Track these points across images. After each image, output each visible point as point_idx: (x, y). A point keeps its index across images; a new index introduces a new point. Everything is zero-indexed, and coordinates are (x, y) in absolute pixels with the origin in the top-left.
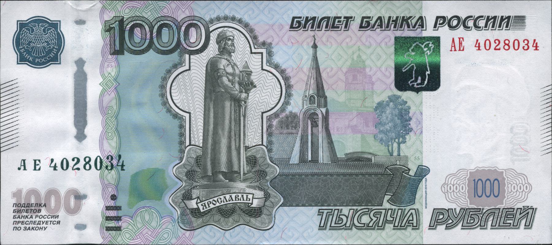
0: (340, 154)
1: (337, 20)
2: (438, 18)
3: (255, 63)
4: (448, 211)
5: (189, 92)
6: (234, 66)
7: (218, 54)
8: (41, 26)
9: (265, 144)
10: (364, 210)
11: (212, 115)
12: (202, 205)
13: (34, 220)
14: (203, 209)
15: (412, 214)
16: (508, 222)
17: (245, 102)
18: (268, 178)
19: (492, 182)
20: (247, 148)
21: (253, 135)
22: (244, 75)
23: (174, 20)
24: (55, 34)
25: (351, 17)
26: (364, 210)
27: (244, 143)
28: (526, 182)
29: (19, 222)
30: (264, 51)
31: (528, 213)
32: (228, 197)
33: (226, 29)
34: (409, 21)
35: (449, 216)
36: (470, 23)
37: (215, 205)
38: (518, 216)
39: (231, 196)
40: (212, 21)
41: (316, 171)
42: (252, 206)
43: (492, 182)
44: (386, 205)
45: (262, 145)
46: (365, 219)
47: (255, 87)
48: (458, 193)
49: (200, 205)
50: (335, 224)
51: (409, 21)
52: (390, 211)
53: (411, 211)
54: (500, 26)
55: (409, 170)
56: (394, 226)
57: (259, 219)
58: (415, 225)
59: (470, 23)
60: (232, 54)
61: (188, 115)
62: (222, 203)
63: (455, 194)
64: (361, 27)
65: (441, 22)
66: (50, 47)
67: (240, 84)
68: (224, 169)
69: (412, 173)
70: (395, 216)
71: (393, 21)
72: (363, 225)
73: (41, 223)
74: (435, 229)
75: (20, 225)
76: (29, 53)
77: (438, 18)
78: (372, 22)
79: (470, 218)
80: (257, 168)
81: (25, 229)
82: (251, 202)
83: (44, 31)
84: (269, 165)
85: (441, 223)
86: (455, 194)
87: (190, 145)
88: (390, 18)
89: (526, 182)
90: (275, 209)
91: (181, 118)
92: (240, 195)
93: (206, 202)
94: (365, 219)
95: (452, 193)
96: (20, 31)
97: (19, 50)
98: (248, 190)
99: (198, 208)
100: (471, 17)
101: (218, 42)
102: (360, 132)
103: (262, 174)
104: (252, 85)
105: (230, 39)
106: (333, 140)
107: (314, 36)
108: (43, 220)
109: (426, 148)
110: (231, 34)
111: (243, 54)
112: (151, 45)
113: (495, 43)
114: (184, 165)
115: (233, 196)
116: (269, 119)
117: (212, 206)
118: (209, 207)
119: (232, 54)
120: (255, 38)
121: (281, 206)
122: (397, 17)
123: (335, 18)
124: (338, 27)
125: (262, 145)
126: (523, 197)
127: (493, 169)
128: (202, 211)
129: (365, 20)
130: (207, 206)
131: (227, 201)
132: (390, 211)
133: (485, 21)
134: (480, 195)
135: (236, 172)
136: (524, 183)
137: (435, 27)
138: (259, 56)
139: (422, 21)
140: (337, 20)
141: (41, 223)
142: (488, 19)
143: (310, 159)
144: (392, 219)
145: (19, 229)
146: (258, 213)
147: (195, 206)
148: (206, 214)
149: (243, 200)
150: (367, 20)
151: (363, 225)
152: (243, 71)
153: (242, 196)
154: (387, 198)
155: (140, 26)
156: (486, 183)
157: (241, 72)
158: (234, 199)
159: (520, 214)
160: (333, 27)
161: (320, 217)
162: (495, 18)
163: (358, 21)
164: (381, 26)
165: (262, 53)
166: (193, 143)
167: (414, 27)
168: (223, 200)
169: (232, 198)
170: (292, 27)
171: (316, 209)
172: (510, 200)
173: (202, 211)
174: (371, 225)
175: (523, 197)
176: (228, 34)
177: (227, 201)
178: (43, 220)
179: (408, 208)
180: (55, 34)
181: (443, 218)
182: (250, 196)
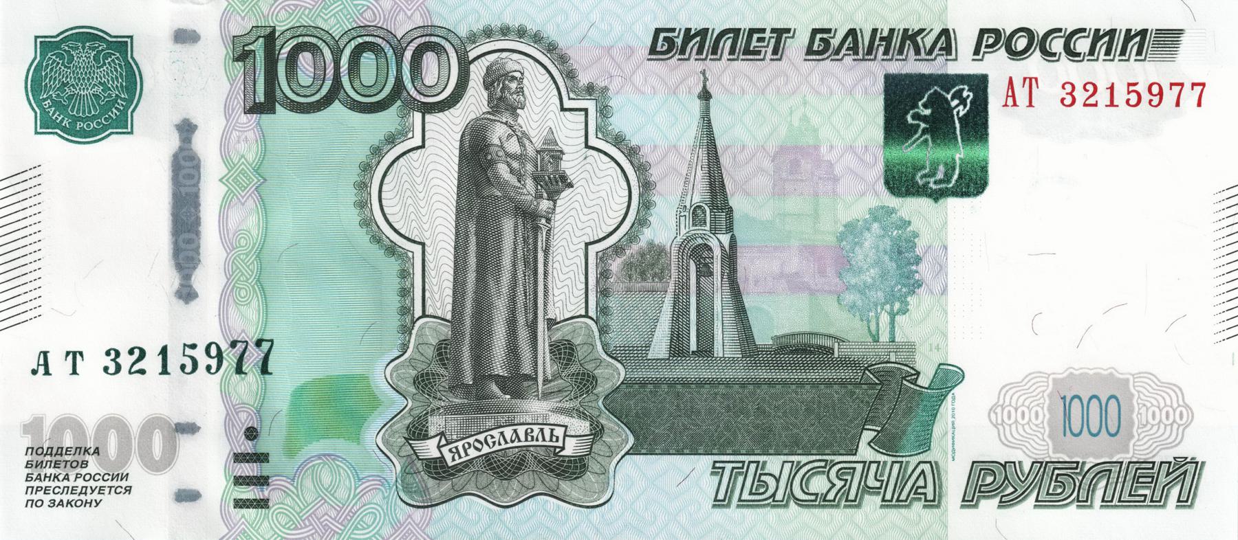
2: (983, 32)
3: (569, 132)
4: (1004, 467)
6: (522, 138)
7: (488, 113)
9: (592, 313)
10: (816, 464)
12: (450, 450)
13: (71, 484)
14: (454, 459)
15: (923, 472)
16: (1141, 492)
17: (548, 220)
18: (599, 389)
20: (551, 323)
22: (547, 158)
24: (120, 66)
25: (788, 31)
26: (816, 464)
27: (545, 313)
29: (38, 489)
30: (590, 105)
31: (1185, 473)
32: (508, 432)
33: (504, 55)
35: (1006, 477)
38: (1163, 480)
39: (515, 431)
40: (473, 38)
44: (865, 452)
46: (819, 484)
47: (570, 185)
49: (445, 450)
51: (919, 39)
52: (874, 466)
54: (1123, 53)
55: (918, 373)
56: (883, 500)
57: (579, 482)
58: (930, 497)
59: (1057, 45)
60: (519, 111)
62: (497, 447)
63: (1020, 427)
64: (810, 51)
65: (991, 41)
67: (536, 179)
68: (499, 369)
69: (924, 381)
70: (885, 478)
71: (882, 39)
72: (813, 498)
73: (89, 491)
74: (976, 506)
75: (40, 495)
77: (983, 32)
78: (835, 42)
79: (1061, 483)
82: (560, 444)
83: (96, 58)
86: (1020, 427)
87: (424, 315)
88: (875, 31)
90: (615, 461)
92: (536, 428)
93: (460, 444)
94: (819, 484)
99: (443, 457)
100: (1060, 30)
101: (488, 85)
104: (564, 182)
105: (514, 78)
106: (747, 305)
107: (704, 73)
110: (517, 67)
111: (542, 114)
113: (1087, 91)
114: (410, 359)
115: (521, 430)
116: (603, 258)
117: (473, 453)
118: (467, 455)
119: (519, 111)
120: (570, 75)
121: (627, 453)
122: (892, 31)
123: (752, 31)
124: (759, 53)
125: (586, 316)
128: (450, 464)
129: (819, 36)
130: (463, 454)
132: (874, 466)
135: (527, 377)
137: (977, 52)
138: (580, 117)
140: (756, 36)
141: (89, 491)
142: (1097, 36)
143: (693, 347)
145: (39, 503)
147: (436, 454)
148: (461, 470)
149: (544, 440)
150: (825, 36)
151: (813, 498)
152: (543, 151)
153: (542, 430)
154: (867, 436)
158: (522, 437)
159: (1168, 474)
160: (747, 51)
161: (717, 479)
162: (1112, 32)
163: (803, 38)
164: (854, 49)
165: (586, 110)
166: (429, 311)
167: (930, 52)
168: (500, 438)
169: (517, 436)
171: (709, 460)
172: (1143, 445)
173: (450, 464)
174: (830, 496)
176: (510, 66)
178: (92, 483)
179: (914, 461)
181: (993, 482)
182: (559, 432)
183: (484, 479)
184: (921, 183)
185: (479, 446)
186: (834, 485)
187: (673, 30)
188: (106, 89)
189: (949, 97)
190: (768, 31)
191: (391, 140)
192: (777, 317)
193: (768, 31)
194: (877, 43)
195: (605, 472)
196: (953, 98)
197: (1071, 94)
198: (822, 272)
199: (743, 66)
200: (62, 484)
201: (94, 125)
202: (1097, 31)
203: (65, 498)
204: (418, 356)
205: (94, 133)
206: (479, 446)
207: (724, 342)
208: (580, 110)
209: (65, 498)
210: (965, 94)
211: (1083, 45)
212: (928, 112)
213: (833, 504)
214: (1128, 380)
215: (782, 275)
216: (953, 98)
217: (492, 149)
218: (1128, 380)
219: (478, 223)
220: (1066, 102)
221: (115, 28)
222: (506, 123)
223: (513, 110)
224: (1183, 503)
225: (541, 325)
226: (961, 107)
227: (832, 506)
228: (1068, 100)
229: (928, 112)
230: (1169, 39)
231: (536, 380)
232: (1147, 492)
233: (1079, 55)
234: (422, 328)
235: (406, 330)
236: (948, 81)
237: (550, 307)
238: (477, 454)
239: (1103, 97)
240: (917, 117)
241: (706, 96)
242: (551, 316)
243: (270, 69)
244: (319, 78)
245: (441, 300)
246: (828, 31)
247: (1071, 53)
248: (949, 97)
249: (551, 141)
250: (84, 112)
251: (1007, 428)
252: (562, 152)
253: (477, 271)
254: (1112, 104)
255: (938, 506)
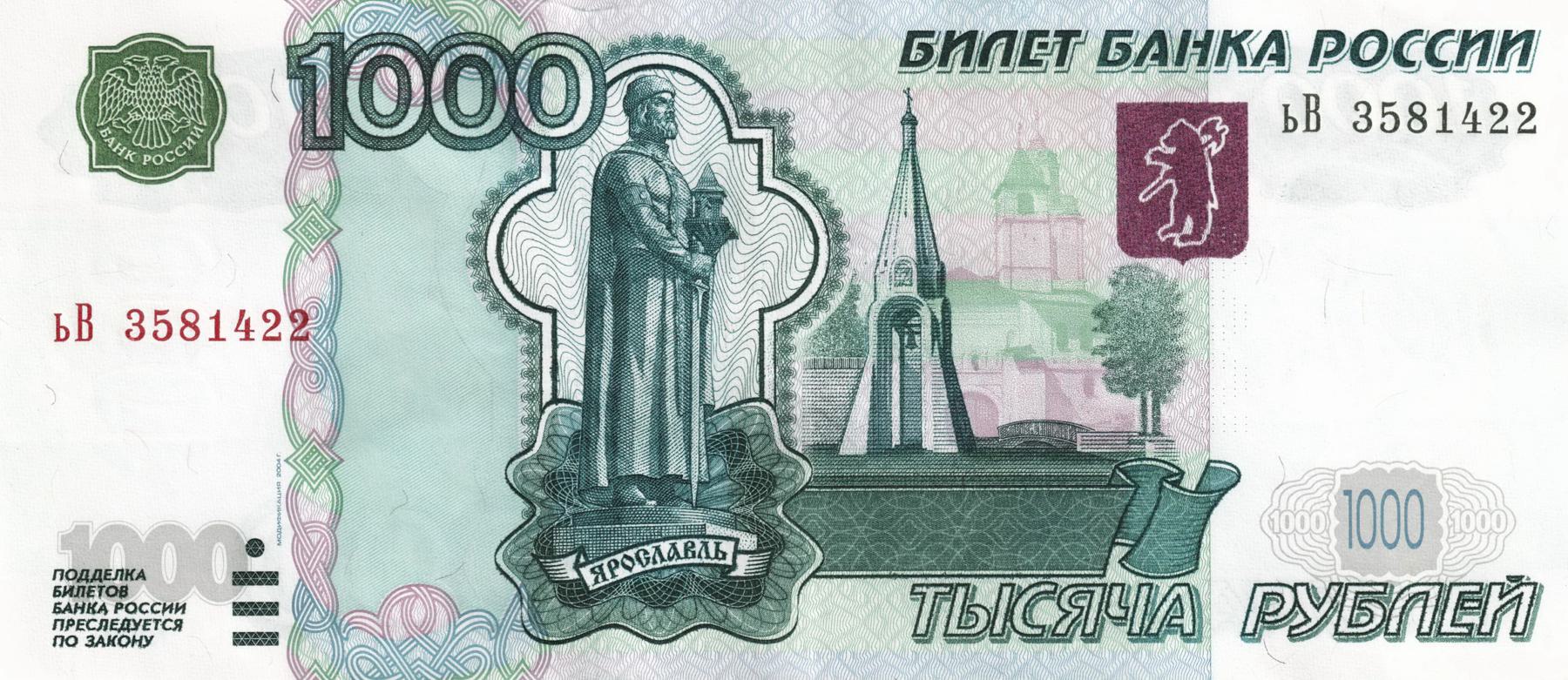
0: (982, 426)
1: (1037, 40)
5: (553, 250)
6: (673, 176)
7: (627, 143)
8: (159, 63)
9: (769, 395)
10: (1042, 588)
11: (608, 318)
12: (592, 570)
13: (111, 616)
14: (596, 581)
15: (1179, 597)
16: (1466, 619)
17: (706, 280)
18: (778, 493)
19: (1378, 503)
20: (708, 409)
21: (730, 372)
22: (704, 201)
23: (495, 47)
24: (197, 85)
25: (1077, 33)
26: (1042, 588)
27: (702, 396)
28: (1501, 505)
29: (71, 623)
31: (1520, 596)
32: (665, 547)
33: (647, 73)
34: (1244, 43)
35: (1296, 603)
36: (1416, 51)
37: (630, 569)
38: (1494, 603)
39: (673, 545)
40: (616, 52)
41: (921, 471)
42: (733, 574)
43: (1378, 503)
44: (1115, 573)
45: (761, 399)
46: (1046, 613)
47: (734, 236)
48: (1307, 537)
49: (586, 571)
50: (1350, 625)
51: (1244, 43)
52: (1117, 590)
53: (1178, 590)
54: (1501, 61)
55: (1182, 473)
56: (1129, 633)
57: (753, 610)
58: (1188, 629)
59: (1416, 51)
60: (668, 142)
61: (767, 315)
62: (650, 566)
63: (1299, 538)
64: (1104, 60)
65: (1332, 47)
66: (184, 123)
68: (641, 467)
69: (1190, 482)
71: (1196, 44)
73: (132, 626)
75: (72, 631)
76: (125, 138)
77: (1321, 35)
78: (1136, 49)
79: (1365, 611)
80: (747, 465)
81: (92, 643)
82: (729, 561)
83: (167, 74)
84: (780, 456)
85: (1273, 625)
86: (1299, 538)
87: (555, 400)
88: (1187, 33)
89: (1501, 505)
91: (534, 328)
92: (698, 542)
94: (1046, 613)
95: (1291, 537)
96: (98, 79)
97: (96, 130)
98: (711, 529)
99: (582, 578)
101: (629, 110)
102: (1038, 364)
103: (760, 484)
104: (728, 232)
105: (664, 101)
106: (963, 389)
107: (907, 91)
108: (138, 616)
109: (1220, 410)
110: (666, 86)
111: (699, 143)
112: (427, 122)
115: (680, 545)
116: (784, 328)
117: (621, 573)
118: (614, 576)
119: (668, 142)
120: (740, 97)
121: (813, 575)
122: (1209, 33)
123: (1032, 34)
125: (761, 399)
126: (1491, 547)
127: (1407, 468)
129: (1116, 40)
130: (608, 575)
131: (663, 560)
132: (1117, 590)
133: (1455, 48)
134: (1367, 540)
135: (678, 478)
136: (1493, 507)
137: (1314, 60)
138: (753, 150)
139: (1281, 46)
140: (1037, 40)
141: (132, 626)
142: (1467, 40)
143: (896, 441)
144: (1121, 613)
145: (71, 641)
146: (740, 592)
147: (573, 575)
148: (604, 596)
149: (708, 557)
150: (1122, 40)
151: (1039, 631)
152: (701, 192)
154: (1118, 552)
155: (555, 60)
156: (1384, 505)
157: (692, 193)
160: (1026, 61)
161: (918, 604)
162: (1487, 35)
163: (1095, 44)
164: (1162, 58)
165: (760, 142)
169: (677, 553)
170: (905, 61)
172: (1466, 557)
174: (1061, 629)
175: (1491, 547)
177: (663, 560)
178: (138, 616)
180: (197, 85)
181: (1271, 612)
182: (727, 547)
183: (633, 607)
184: (1163, 239)
185: (628, 563)
186: (1068, 613)
187: (930, 34)
188: (180, 114)
189: (1198, 131)
190: (1052, 34)
191: (514, 181)
192: (1008, 400)
193: (1052, 34)
194: (1190, 49)
195: (786, 597)
196: (1204, 131)
197: (1366, 116)
198: (1062, 345)
199: (1021, 79)
200: (99, 617)
201: (165, 158)
202: (1467, 33)
203: (105, 635)
204: (548, 451)
205: (167, 168)
206: (628, 563)
207: (936, 435)
208: (752, 141)
209: (105, 635)
210: (1218, 128)
211: (1448, 50)
212: (1171, 150)
213: (1065, 638)
214: (1434, 477)
215: (1008, 350)
216: (1204, 131)
217: (634, 192)
218: (1434, 477)
219: (614, 287)
220: (1388, 127)
221: (191, 36)
222: (653, 158)
223: (662, 139)
224: (1518, 635)
225: (697, 413)
226: (1213, 144)
227: (1064, 641)
228: (136, 332)
229: (1171, 150)
230: (1522, 43)
231: (689, 482)
232: (1475, 620)
233: (1444, 63)
234: (553, 416)
235: (533, 421)
236: (1198, 111)
237: (708, 392)
238: (627, 573)
239: (207, 327)
240: (1158, 156)
241: (910, 121)
242: (708, 400)
243: (337, 91)
244: (404, 101)
245: (573, 384)
246: (1128, 33)
247: (1432, 60)
248: (1198, 131)
249: (708, 178)
250: (152, 144)
251: (1283, 538)
252: (723, 194)
253: (614, 341)
254: (217, 338)
255: (1199, 640)
